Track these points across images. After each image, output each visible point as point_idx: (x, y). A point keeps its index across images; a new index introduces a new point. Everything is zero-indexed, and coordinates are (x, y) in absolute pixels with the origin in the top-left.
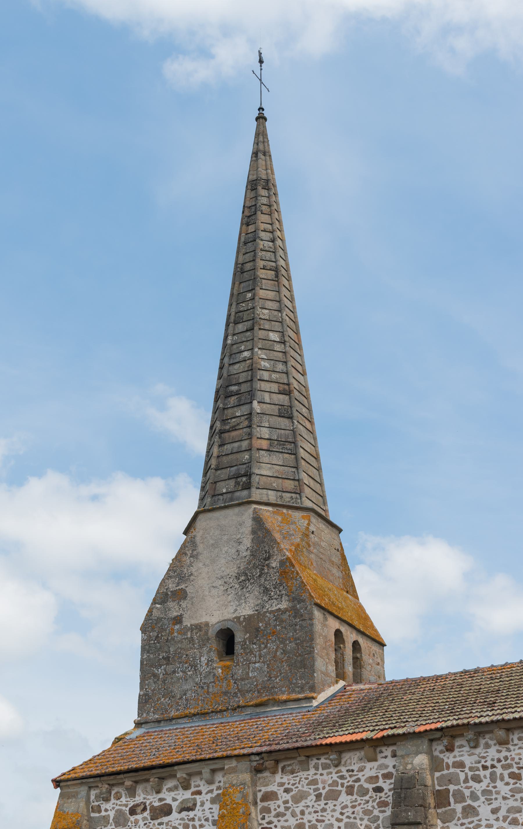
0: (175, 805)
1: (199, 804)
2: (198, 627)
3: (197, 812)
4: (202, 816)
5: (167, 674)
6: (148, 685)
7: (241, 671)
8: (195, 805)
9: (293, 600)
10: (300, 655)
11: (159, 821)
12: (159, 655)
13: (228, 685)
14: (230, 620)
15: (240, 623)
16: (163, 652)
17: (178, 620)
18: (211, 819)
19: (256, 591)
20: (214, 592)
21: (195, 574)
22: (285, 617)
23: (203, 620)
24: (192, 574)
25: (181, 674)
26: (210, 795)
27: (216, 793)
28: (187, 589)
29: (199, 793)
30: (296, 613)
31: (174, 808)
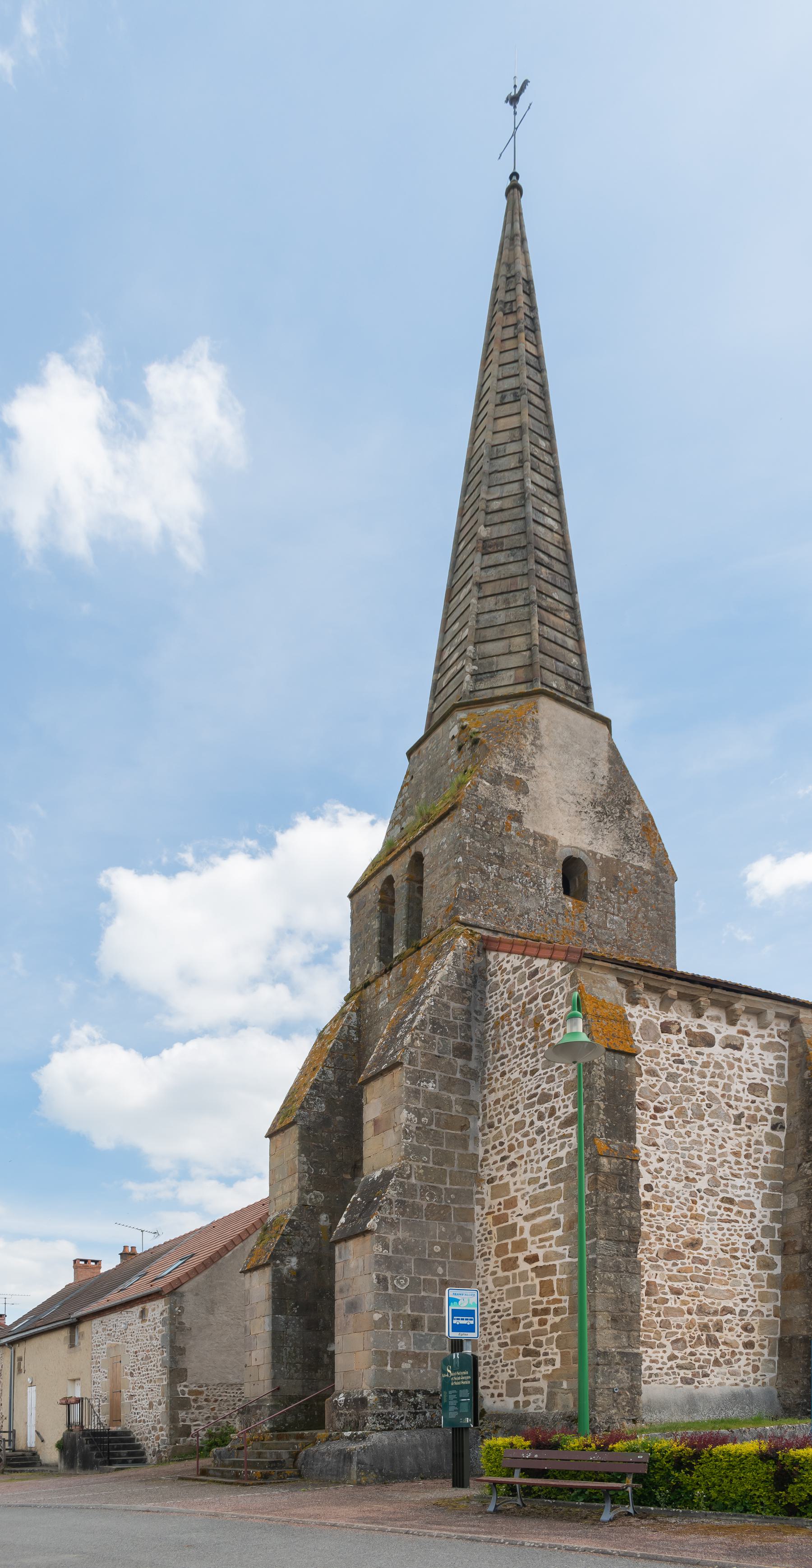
0: (718, 1038)
1: (746, 1046)
2: (544, 840)
3: (744, 1053)
4: (750, 1060)
5: (499, 876)
6: (473, 879)
7: (596, 916)
8: (742, 1045)
9: (656, 865)
10: (662, 928)
11: (698, 1049)
12: (489, 848)
13: (582, 926)
14: (584, 851)
15: (597, 861)
16: (494, 847)
17: (517, 816)
18: (760, 1065)
19: (616, 833)
20: (563, 805)
21: (539, 770)
22: (648, 879)
23: (551, 833)
24: (533, 768)
25: (519, 886)
26: (759, 1040)
27: (767, 1040)
28: (529, 783)
29: (747, 1034)
30: (658, 882)
31: (717, 1041)
